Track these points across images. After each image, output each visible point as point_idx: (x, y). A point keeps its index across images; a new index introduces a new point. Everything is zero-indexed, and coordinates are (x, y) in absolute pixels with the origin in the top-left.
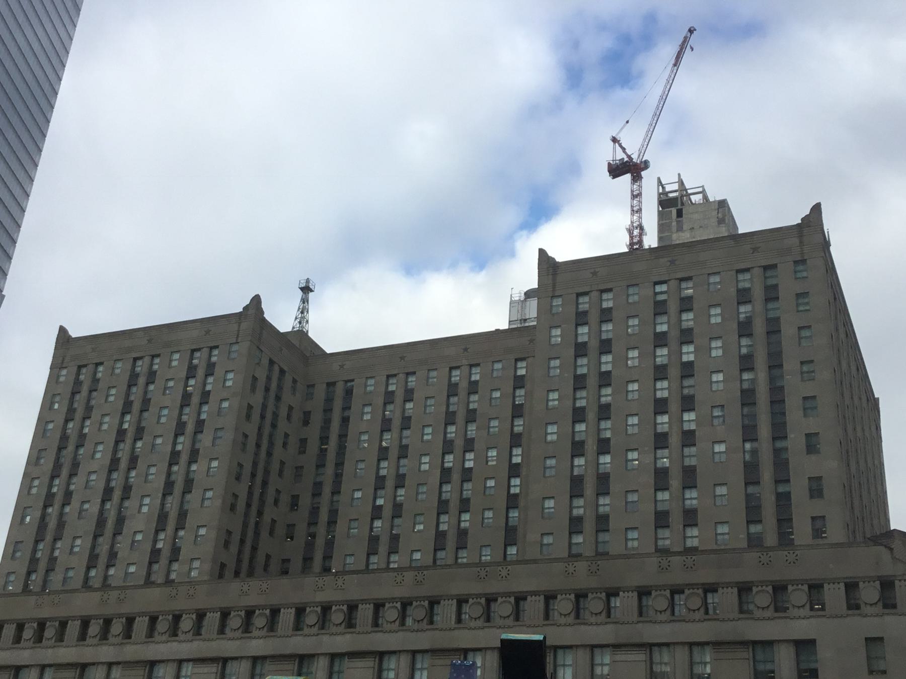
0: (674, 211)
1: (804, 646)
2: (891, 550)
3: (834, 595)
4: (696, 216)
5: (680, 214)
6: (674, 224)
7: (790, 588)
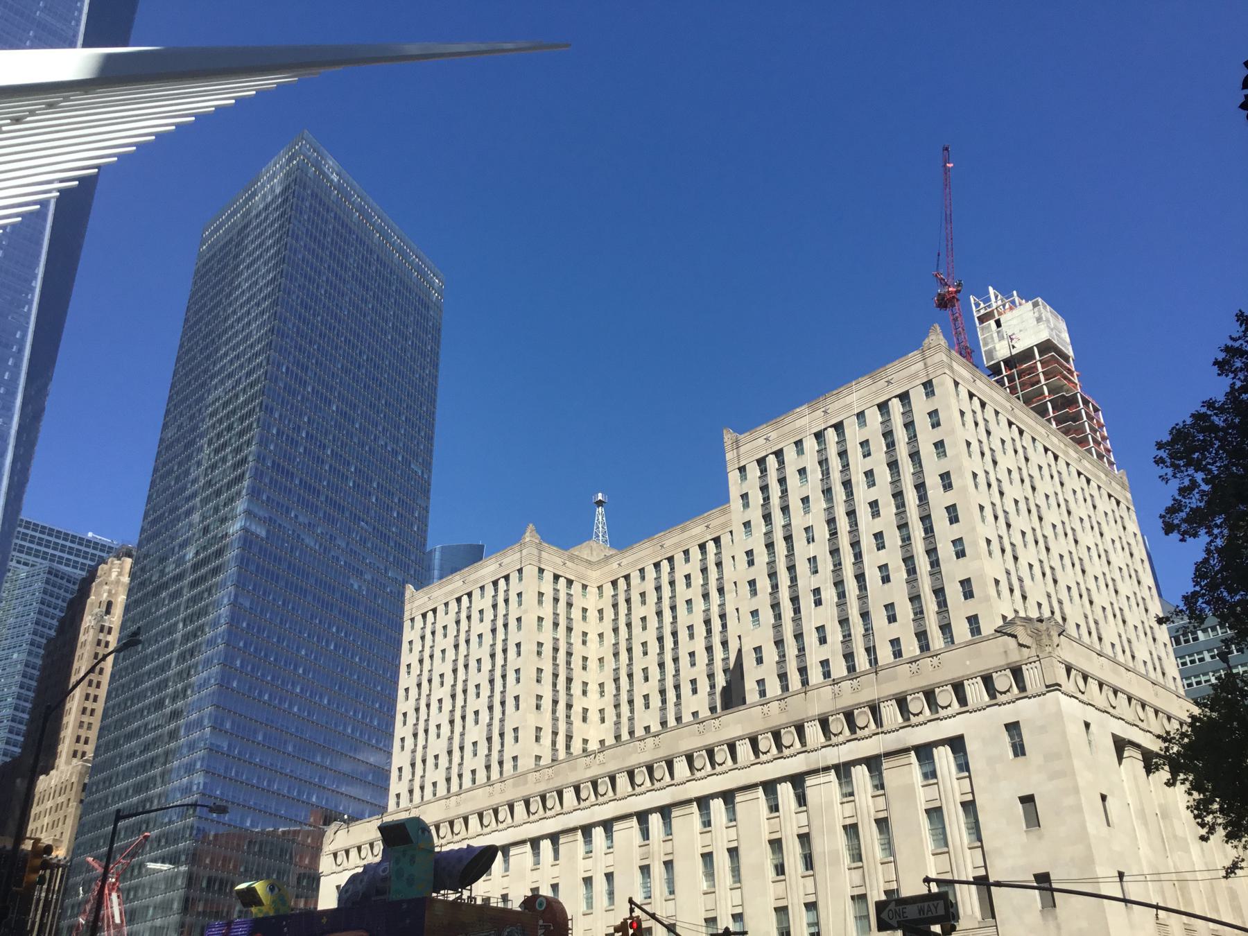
0: (992, 322)
1: (957, 744)
2: (1015, 637)
3: (976, 692)
4: (1015, 322)
5: (998, 324)
6: (995, 335)
7: (937, 690)
